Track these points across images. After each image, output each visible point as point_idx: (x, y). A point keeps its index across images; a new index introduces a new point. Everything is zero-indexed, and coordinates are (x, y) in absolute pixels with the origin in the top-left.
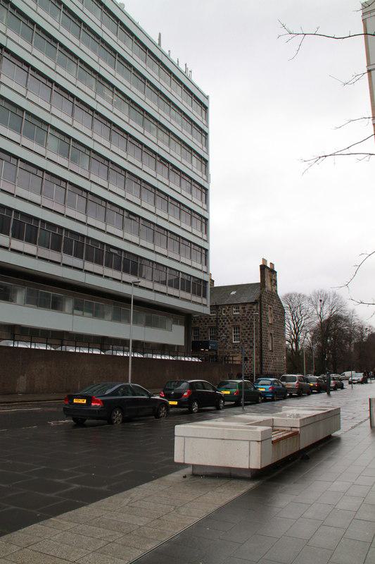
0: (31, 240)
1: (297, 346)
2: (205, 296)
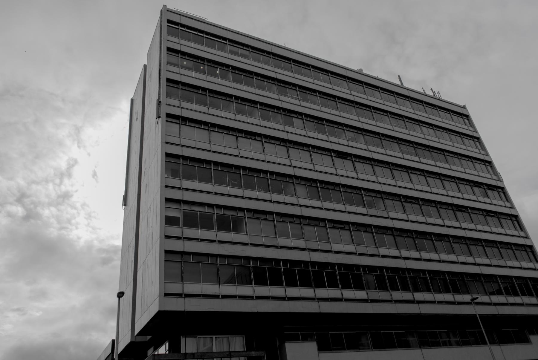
0: (359, 286)
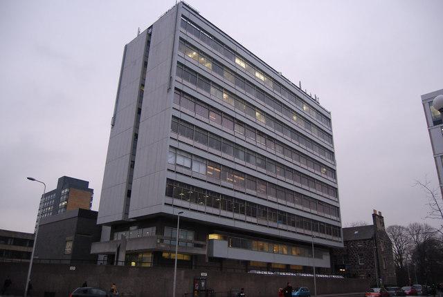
1: (401, 263)
2: (340, 236)
